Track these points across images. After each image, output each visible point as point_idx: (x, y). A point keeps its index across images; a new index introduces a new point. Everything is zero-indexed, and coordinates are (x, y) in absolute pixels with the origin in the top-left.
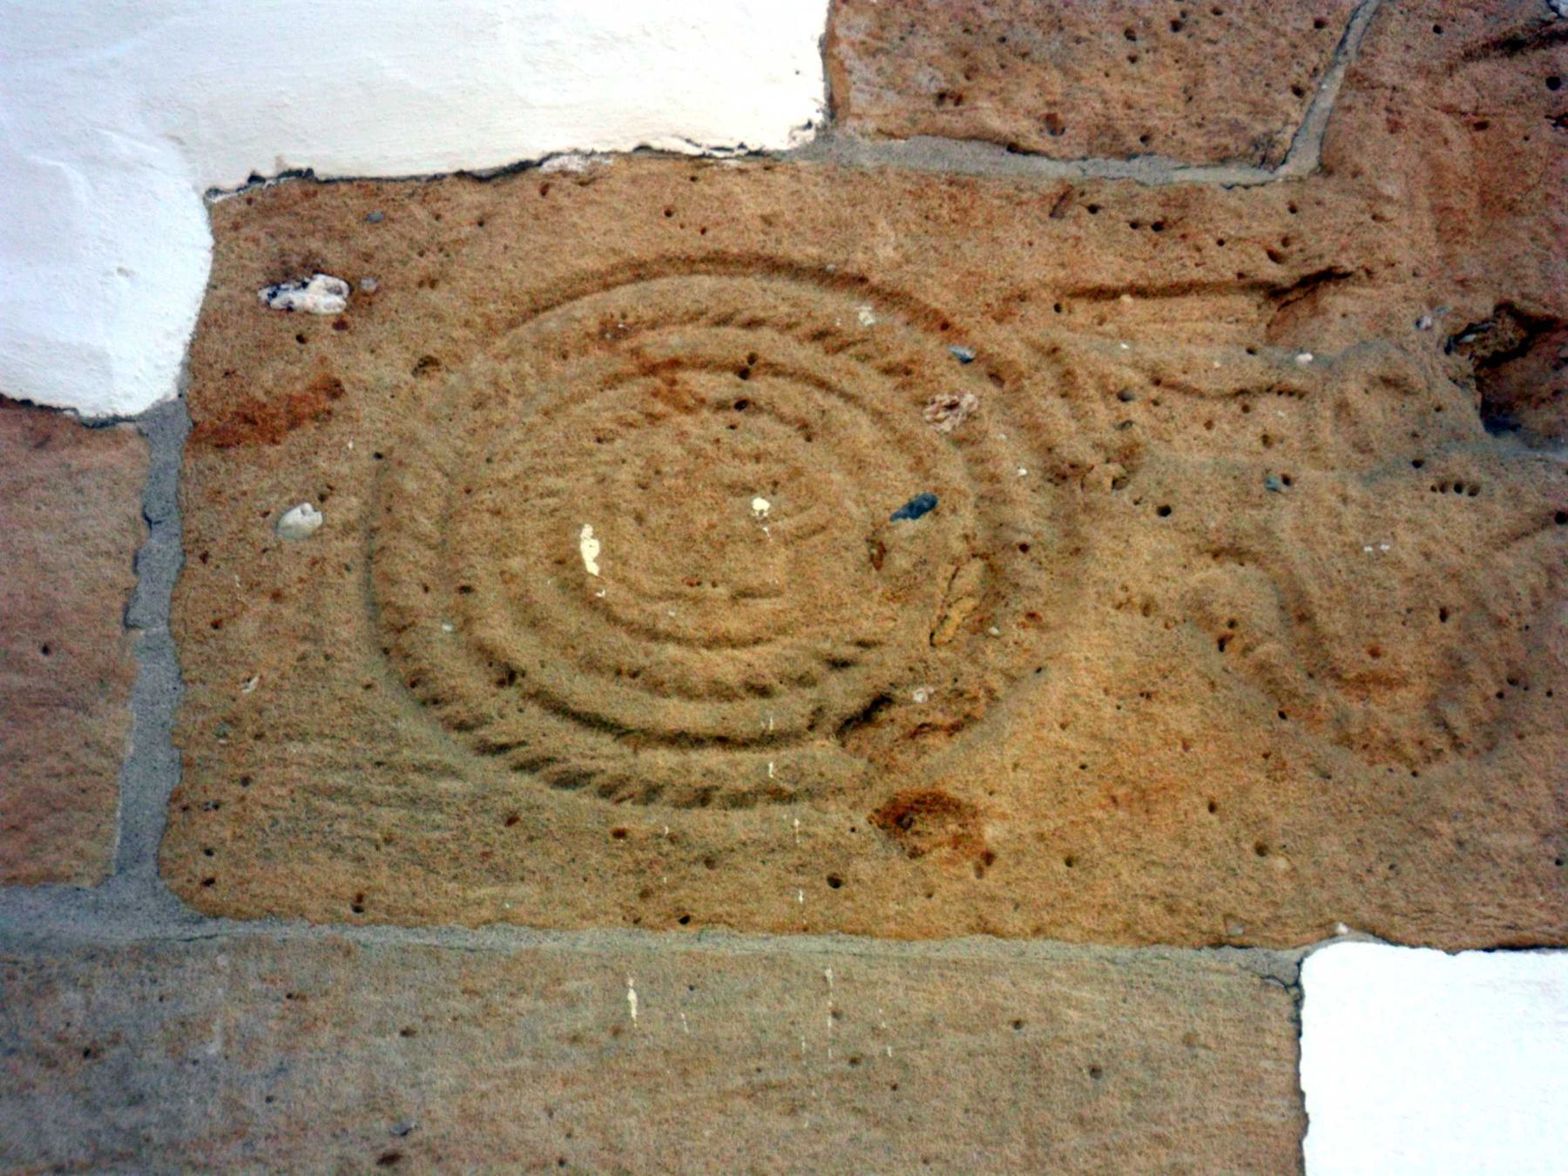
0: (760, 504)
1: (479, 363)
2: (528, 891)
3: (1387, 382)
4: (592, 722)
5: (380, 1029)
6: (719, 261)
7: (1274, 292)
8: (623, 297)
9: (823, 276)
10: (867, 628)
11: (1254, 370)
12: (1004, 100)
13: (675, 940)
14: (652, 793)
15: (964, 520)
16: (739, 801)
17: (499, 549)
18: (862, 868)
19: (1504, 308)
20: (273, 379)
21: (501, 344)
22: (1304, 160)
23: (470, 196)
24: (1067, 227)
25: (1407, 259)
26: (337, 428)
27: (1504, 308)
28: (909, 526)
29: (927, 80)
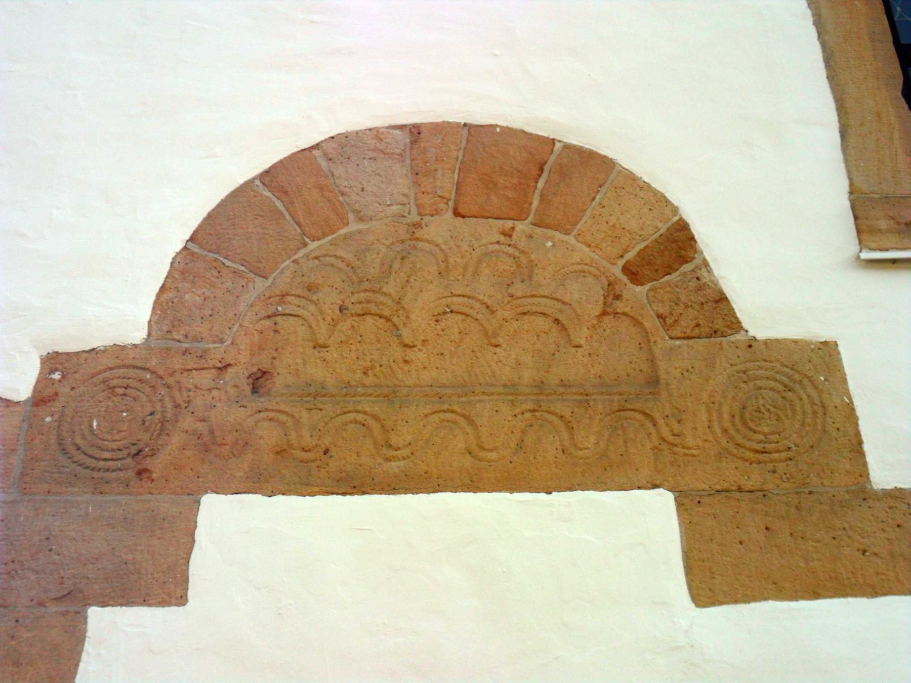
0: (125, 414)
1: (82, 388)
2: (76, 489)
3: (235, 386)
4: (91, 457)
5: (49, 515)
6: (125, 366)
7: (219, 368)
8: (107, 374)
9: (141, 368)
10: (139, 437)
11: (212, 385)
12: (178, 332)
13: (99, 497)
14: (99, 470)
15: (158, 416)
16: (114, 471)
17: (80, 424)
18: (132, 483)
19: (259, 369)
20: (48, 392)
21: (86, 384)
22: (229, 342)
23: (84, 355)
24: (185, 357)
25: (243, 361)
26: (56, 402)
27: (259, 369)
28: (149, 417)
29: (165, 329)
